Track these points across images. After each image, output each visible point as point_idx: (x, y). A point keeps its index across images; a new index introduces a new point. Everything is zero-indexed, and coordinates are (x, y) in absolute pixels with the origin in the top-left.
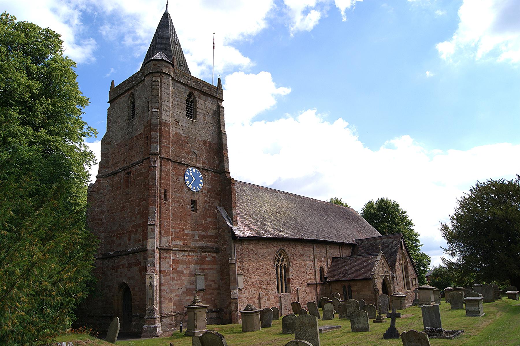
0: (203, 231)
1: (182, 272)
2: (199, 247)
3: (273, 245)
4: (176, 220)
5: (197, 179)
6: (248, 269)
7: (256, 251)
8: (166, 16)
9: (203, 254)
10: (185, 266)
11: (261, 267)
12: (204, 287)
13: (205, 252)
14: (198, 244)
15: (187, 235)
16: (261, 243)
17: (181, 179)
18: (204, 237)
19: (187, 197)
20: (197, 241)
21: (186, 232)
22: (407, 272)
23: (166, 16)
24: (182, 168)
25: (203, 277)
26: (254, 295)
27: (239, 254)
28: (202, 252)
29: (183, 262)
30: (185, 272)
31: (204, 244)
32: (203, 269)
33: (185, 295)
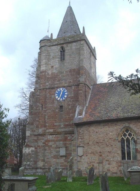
0: (67, 122)
1: (51, 146)
2: (63, 132)
3: (115, 124)
4: (49, 119)
5: (64, 94)
6: (88, 143)
7: (97, 130)
8: (70, 13)
9: (66, 135)
10: (53, 143)
11: (101, 141)
12: (65, 155)
13: (67, 134)
14: (63, 130)
15: (56, 126)
16: (102, 125)
17: (53, 96)
18: (67, 125)
19: (56, 104)
20: (62, 128)
21: (55, 124)
22: (122, 154)
23: (70, 13)
24: (53, 90)
25: (64, 149)
26: (94, 161)
27: (81, 134)
28: (65, 134)
29: (52, 141)
30: (53, 146)
31: (67, 130)
32: (65, 144)
33: (53, 158)
